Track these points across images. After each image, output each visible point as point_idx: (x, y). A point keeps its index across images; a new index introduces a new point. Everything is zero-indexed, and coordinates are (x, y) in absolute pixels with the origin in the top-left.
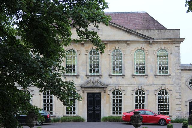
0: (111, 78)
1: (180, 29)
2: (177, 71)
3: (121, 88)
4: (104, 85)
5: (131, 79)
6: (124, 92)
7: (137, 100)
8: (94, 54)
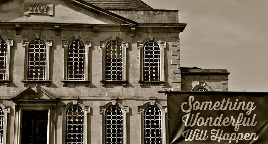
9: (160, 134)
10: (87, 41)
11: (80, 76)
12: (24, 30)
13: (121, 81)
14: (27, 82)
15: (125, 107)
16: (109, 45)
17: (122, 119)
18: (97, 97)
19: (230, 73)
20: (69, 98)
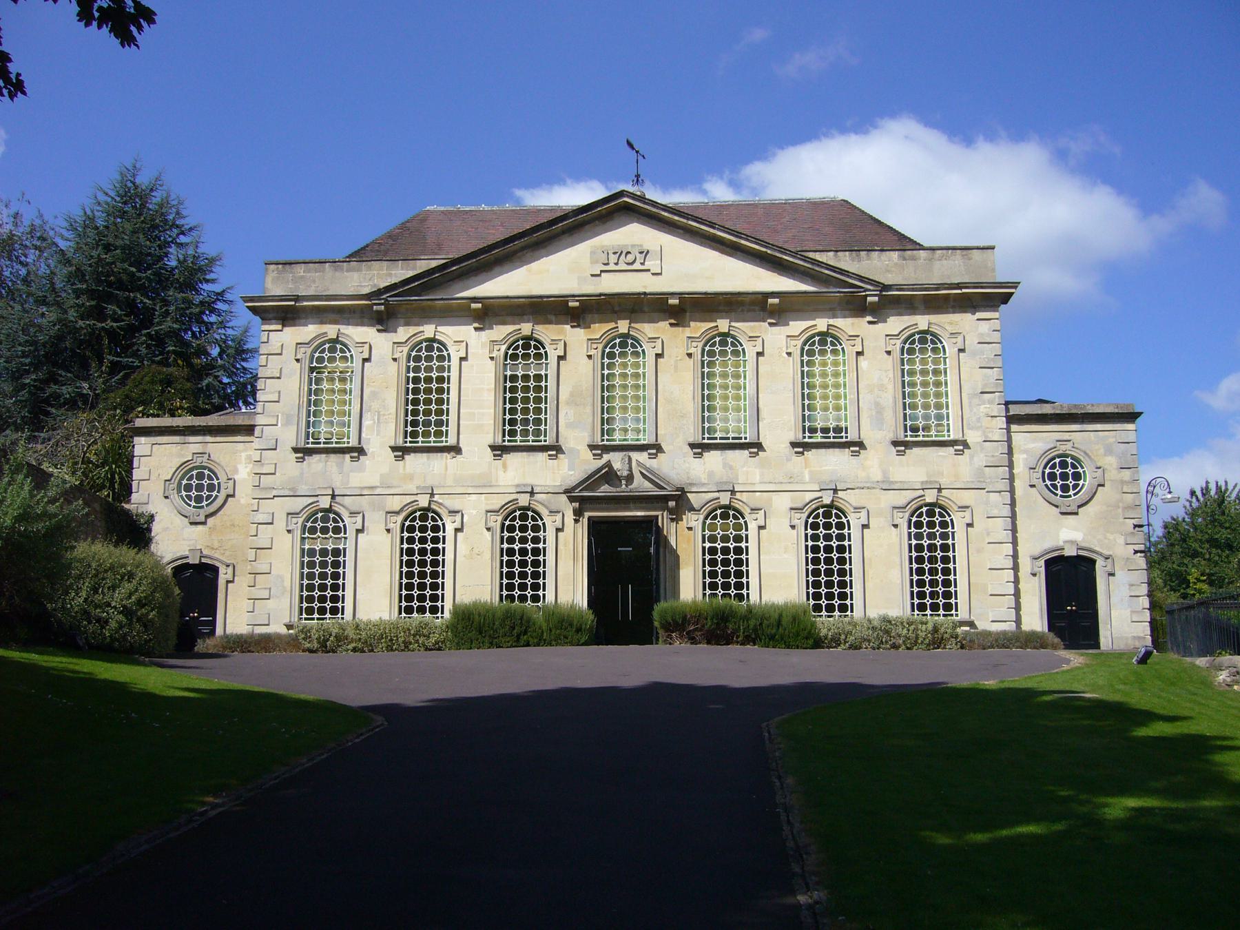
0: (900, 454)
1: (993, 248)
2: (986, 422)
3: (744, 497)
4: (668, 483)
5: (789, 460)
6: (754, 516)
7: (511, 552)
8: (923, 351)
9: (848, 581)
10: (750, 337)
11: (537, 433)
12: (590, 316)
13: (844, 440)
14: (600, 447)
15: (752, 510)
16: (909, 344)
17: (850, 540)
18: (782, 483)
19: (1142, 413)
20: (710, 486)
